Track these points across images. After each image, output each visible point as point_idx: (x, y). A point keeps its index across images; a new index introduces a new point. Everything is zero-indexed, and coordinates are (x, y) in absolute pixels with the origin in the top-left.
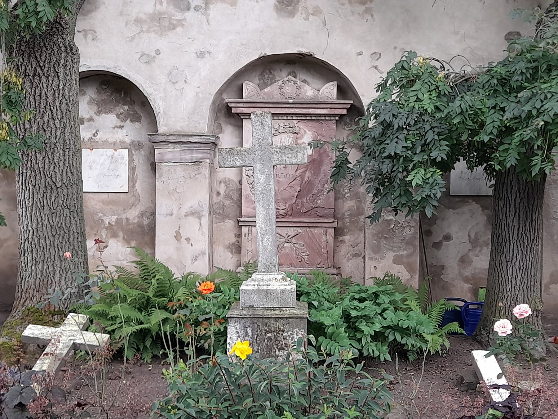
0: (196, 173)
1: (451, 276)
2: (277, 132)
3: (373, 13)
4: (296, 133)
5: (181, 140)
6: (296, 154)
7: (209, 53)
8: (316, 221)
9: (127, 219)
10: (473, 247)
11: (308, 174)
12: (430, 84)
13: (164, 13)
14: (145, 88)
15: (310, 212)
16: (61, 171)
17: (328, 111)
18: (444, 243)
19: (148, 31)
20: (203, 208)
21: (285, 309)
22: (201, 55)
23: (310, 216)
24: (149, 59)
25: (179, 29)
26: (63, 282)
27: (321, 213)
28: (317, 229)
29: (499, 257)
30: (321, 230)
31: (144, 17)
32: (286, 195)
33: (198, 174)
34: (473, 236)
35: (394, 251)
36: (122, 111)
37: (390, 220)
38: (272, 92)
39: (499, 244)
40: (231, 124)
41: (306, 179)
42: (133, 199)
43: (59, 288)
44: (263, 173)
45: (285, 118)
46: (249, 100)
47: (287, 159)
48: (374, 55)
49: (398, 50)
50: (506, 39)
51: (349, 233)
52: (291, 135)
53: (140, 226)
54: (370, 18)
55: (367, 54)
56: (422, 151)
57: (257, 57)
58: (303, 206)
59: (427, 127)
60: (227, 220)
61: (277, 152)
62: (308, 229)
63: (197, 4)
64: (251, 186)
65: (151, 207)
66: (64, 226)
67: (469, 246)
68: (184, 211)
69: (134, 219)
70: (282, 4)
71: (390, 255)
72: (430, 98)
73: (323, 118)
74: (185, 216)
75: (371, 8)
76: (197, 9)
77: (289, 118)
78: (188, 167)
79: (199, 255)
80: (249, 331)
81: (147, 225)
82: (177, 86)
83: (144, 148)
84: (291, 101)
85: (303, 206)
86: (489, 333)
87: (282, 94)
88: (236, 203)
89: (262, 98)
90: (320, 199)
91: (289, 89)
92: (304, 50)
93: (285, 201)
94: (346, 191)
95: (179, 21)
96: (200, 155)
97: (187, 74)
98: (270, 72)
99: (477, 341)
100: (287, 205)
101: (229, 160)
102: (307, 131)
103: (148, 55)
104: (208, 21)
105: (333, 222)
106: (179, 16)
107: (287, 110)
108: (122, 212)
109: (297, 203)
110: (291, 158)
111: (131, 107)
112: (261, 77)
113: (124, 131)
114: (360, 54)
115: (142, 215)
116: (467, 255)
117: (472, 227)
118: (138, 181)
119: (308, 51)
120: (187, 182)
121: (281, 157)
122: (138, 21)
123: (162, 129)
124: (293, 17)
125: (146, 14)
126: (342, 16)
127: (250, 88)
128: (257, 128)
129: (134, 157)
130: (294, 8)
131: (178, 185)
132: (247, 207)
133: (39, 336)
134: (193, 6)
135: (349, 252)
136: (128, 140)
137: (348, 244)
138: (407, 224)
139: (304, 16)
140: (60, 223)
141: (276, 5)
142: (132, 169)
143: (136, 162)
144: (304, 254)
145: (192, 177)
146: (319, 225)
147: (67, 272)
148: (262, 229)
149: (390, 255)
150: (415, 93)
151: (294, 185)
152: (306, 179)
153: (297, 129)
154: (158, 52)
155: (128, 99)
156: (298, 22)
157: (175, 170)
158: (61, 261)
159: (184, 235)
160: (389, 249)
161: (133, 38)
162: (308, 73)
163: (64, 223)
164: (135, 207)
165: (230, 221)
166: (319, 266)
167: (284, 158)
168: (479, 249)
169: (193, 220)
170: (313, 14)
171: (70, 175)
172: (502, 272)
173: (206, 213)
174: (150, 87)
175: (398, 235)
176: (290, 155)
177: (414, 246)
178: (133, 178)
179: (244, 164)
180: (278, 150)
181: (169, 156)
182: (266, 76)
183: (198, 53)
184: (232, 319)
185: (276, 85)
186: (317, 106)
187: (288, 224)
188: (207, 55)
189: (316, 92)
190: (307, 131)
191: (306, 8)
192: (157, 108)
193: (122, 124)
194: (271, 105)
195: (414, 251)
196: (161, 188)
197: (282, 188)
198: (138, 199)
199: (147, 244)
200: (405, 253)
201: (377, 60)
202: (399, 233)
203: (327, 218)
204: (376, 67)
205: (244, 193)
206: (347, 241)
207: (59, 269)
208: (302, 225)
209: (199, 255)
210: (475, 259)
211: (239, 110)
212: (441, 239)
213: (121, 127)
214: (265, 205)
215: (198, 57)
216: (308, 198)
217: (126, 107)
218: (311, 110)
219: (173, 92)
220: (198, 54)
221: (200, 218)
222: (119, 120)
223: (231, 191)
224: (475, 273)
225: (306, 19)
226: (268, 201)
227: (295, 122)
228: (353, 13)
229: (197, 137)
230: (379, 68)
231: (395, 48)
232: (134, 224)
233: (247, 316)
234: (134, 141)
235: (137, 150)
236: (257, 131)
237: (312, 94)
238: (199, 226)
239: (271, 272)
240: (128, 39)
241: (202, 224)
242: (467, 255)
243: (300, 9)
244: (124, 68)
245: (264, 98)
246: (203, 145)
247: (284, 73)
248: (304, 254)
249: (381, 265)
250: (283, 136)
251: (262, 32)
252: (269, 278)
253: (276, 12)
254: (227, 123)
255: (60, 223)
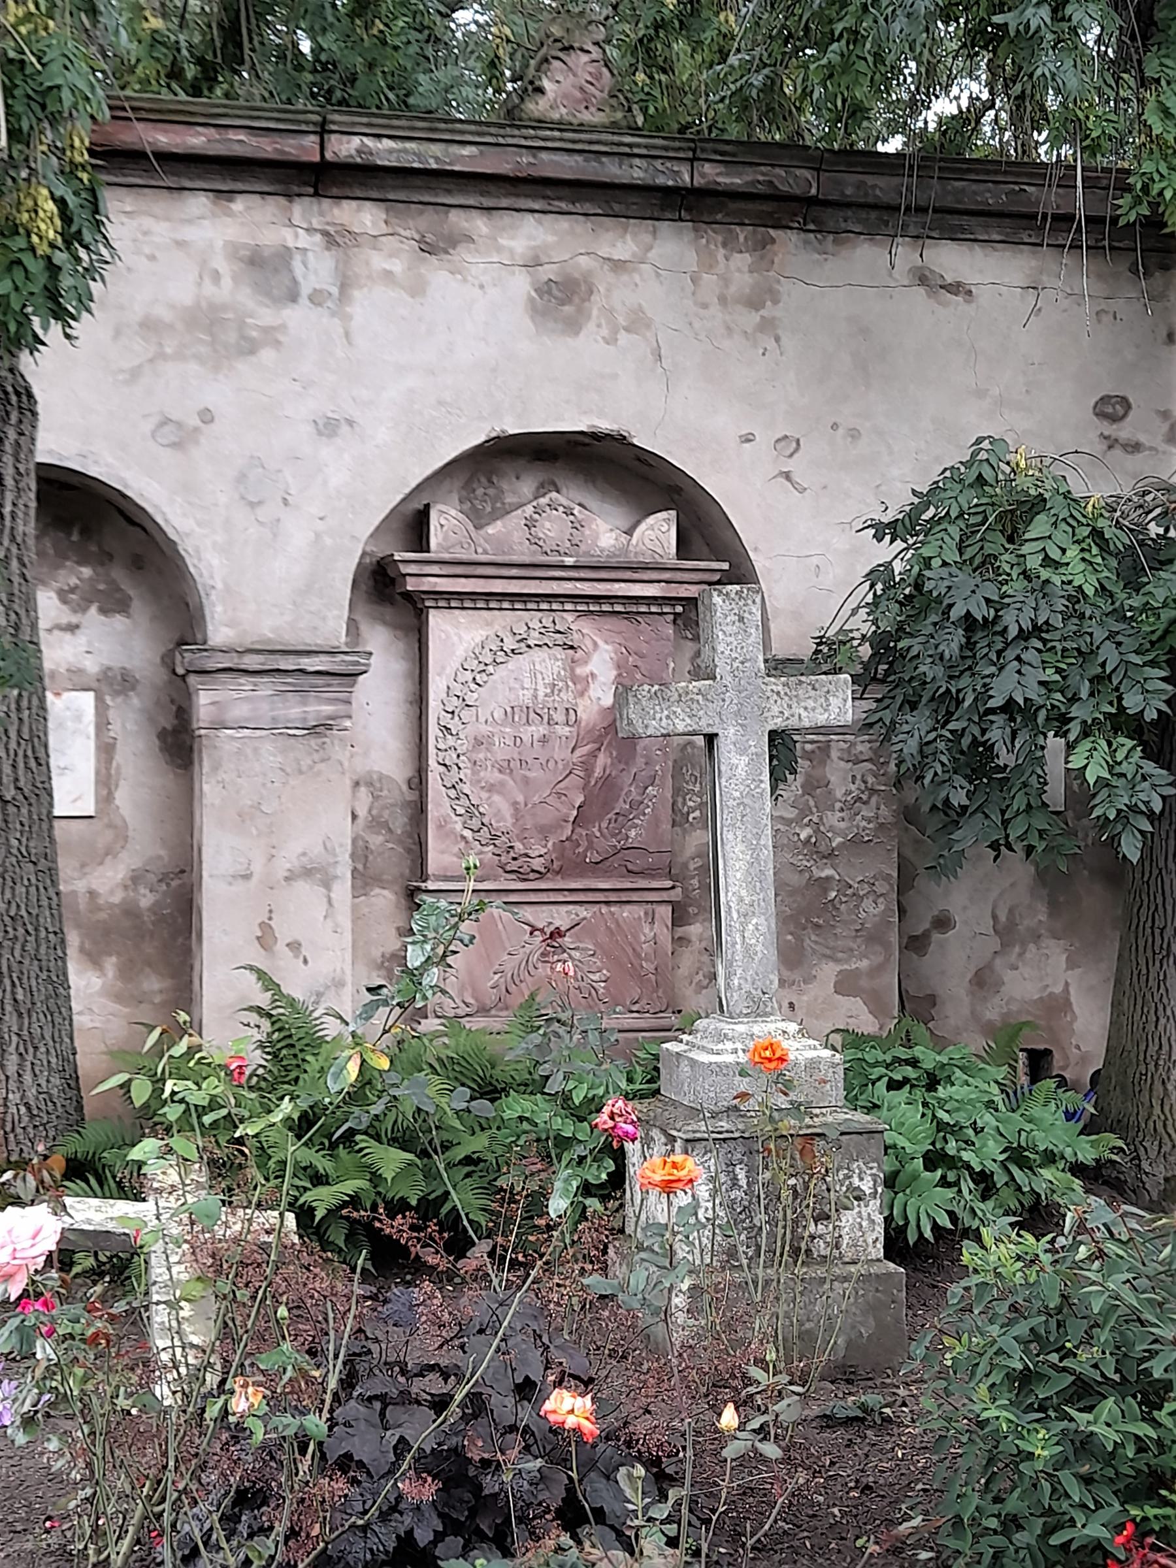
0: (316, 757)
1: (952, 1021)
2: (523, 645)
3: (780, 332)
4: (572, 647)
5: (278, 665)
6: (827, 699)
7: (350, 423)
8: (629, 885)
9: (92, 894)
10: (1006, 945)
11: (602, 759)
12: (1075, 524)
13: (224, 307)
14: (170, 517)
15: (607, 863)
16: (12, 753)
17: (662, 589)
18: (936, 936)
19: (179, 356)
20: (335, 855)
21: (817, 1111)
22: (328, 428)
23: (607, 874)
24: (179, 435)
25: (267, 355)
26: (28, 1077)
27: (638, 863)
28: (628, 907)
29: (1158, 964)
30: (639, 911)
31: (166, 315)
32: (547, 816)
33: (323, 761)
34: (1003, 918)
35: (837, 961)
36: (73, 581)
37: (828, 878)
38: (507, 535)
39: (1157, 932)
40: (385, 623)
41: (598, 772)
42: (109, 835)
43: (18, 1095)
44: (743, 751)
45: (544, 606)
46: (446, 556)
47: (804, 714)
48: (783, 443)
49: (841, 431)
50: (1097, 415)
51: (701, 918)
52: (559, 652)
53: (130, 911)
54: (771, 344)
55: (765, 439)
56: (1092, 694)
57: (482, 438)
58: (591, 846)
59: (1100, 635)
60: (377, 891)
61: (778, 693)
62: (604, 909)
63: (318, 287)
64: (452, 793)
65: (160, 857)
66: (23, 913)
67: (995, 943)
68: (282, 866)
69: (112, 892)
70: (546, 297)
71: (829, 972)
72: (1083, 559)
73: (643, 609)
74: (287, 879)
75: (774, 318)
76: (317, 298)
77: (555, 606)
78: (292, 740)
79: (328, 987)
80: (741, 1175)
81: (149, 909)
82: (261, 513)
83: (139, 688)
84: (569, 561)
85: (591, 846)
86: (1138, 1157)
87: (534, 541)
88: (400, 842)
89: (480, 550)
90: (636, 826)
91: (552, 528)
92: (605, 425)
93: (544, 832)
94: (691, 804)
95: (267, 330)
96: (328, 709)
97: (290, 480)
98: (490, 482)
99: (1105, 1183)
100: (550, 845)
101: (658, 716)
102: (600, 642)
103: (179, 425)
104: (347, 335)
105: (673, 887)
106: (266, 316)
107: (608, 586)
108: (76, 874)
109: (574, 837)
110: (814, 709)
111: (100, 570)
112: (464, 493)
113: (81, 640)
114: (748, 439)
115: (136, 879)
116: (989, 966)
117: (1001, 894)
118: (122, 782)
119: (615, 427)
120: (292, 782)
121: (790, 707)
122: (150, 326)
123: (219, 632)
124: (577, 333)
125: (172, 307)
126: (702, 337)
127: (446, 524)
128: (728, 629)
129: (112, 714)
130: (580, 310)
131: (264, 792)
132: (443, 852)
133: (110, 1226)
134: (305, 290)
135: (700, 968)
136: (92, 666)
137: (697, 945)
138: (867, 887)
139: (605, 332)
140: (14, 905)
141: (531, 300)
142: (106, 750)
143: (115, 729)
144: (596, 977)
145: (304, 768)
146: (635, 897)
147: (36, 1048)
148: (741, 900)
149: (829, 972)
150: (1038, 546)
151: (566, 788)
152: (598, 772)
153: (576, 636)
154: (207, 416)
155: (94, 548)
156: (588, 346)
157: (256, 750)
158: (20, 1015)
159: (284, 932)
160: (824, 956)
161: (135, 374)
162: (590, 485)
163: (23, 906)
164: (115, 857)
165: (386, 892)
166: (635, 1008)
167: (797, 710)
168: (1017, 949)
169: (307, 892)
170: (627, 330)
171: (33, 764)
172: (1165, 1000)
173: (344, 870)
174: (185, 515)
175: (845, 917)
176: (810, 703)
177: (887, 946)
178: (109, 776)
179: (695, 727)
180: (780, 688)
181: (239, 712)
182: (480, 491)
183: (321, 423)
184: (698, 1145)
185: (517, 517)
186: (636, 576)
187: (553, 897)
188: (345, 429)
189: (624, 538)
190: (600, 642)
191: (609, 312)
192: (205, 572)
193: (74, 619)
194: (514, 572)
195: (887, 960)
196: (217, 802)
197: (536, 799)
198: (121, 834)
199: (150, 965)
200: (864, 964)
201: (791, 455)
202: (850, 911)
203: (653, 877)
204: (787, 476)
205: (433, 812)
206: (694, 939)
207: (15, 1038)
208: (591, 897)
209: (328, 987)
210: (1009, 976)
211: (427, 584)
212: (927, 926)
213: (72, 628)
214: (749, 836)
215: (320, 433)
216: (604, 825)
217: (86, 572)
218: (617, 585)
219: (251, 530)
220: (321, 426)
221: (327, 884)
222: (64, 607)
223: (385, 807)
224: (1008, 1014)
225: (611, 341)
226: (757, 824)
227: (570, 617)
228: (729, 328)
229: (323, 658)
230: (796, 477)
231: (835, 426)
232: (112, 906)
233: (737, 1135)
234: (109, 669)
235: (117, 693)
236: (729, 639)
237: (612, 542)
238: (325, 906)
239: (766, 1014)
240: (121, 377)
241: (335, 904)
242: (989, 966)
243: (595, 312)
244: (110, 460)
245: (485, 552)
246: (335, 681)
247: (526, 487)
248: (596, 977)
249: (805, 998)
250: (538, 655)
251: (494, 370)
252: (766, 1030)
253: (532, 318)
254: (374, 619)
255: (14, 905)
